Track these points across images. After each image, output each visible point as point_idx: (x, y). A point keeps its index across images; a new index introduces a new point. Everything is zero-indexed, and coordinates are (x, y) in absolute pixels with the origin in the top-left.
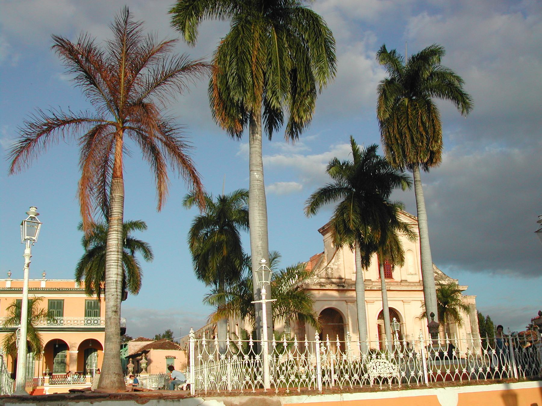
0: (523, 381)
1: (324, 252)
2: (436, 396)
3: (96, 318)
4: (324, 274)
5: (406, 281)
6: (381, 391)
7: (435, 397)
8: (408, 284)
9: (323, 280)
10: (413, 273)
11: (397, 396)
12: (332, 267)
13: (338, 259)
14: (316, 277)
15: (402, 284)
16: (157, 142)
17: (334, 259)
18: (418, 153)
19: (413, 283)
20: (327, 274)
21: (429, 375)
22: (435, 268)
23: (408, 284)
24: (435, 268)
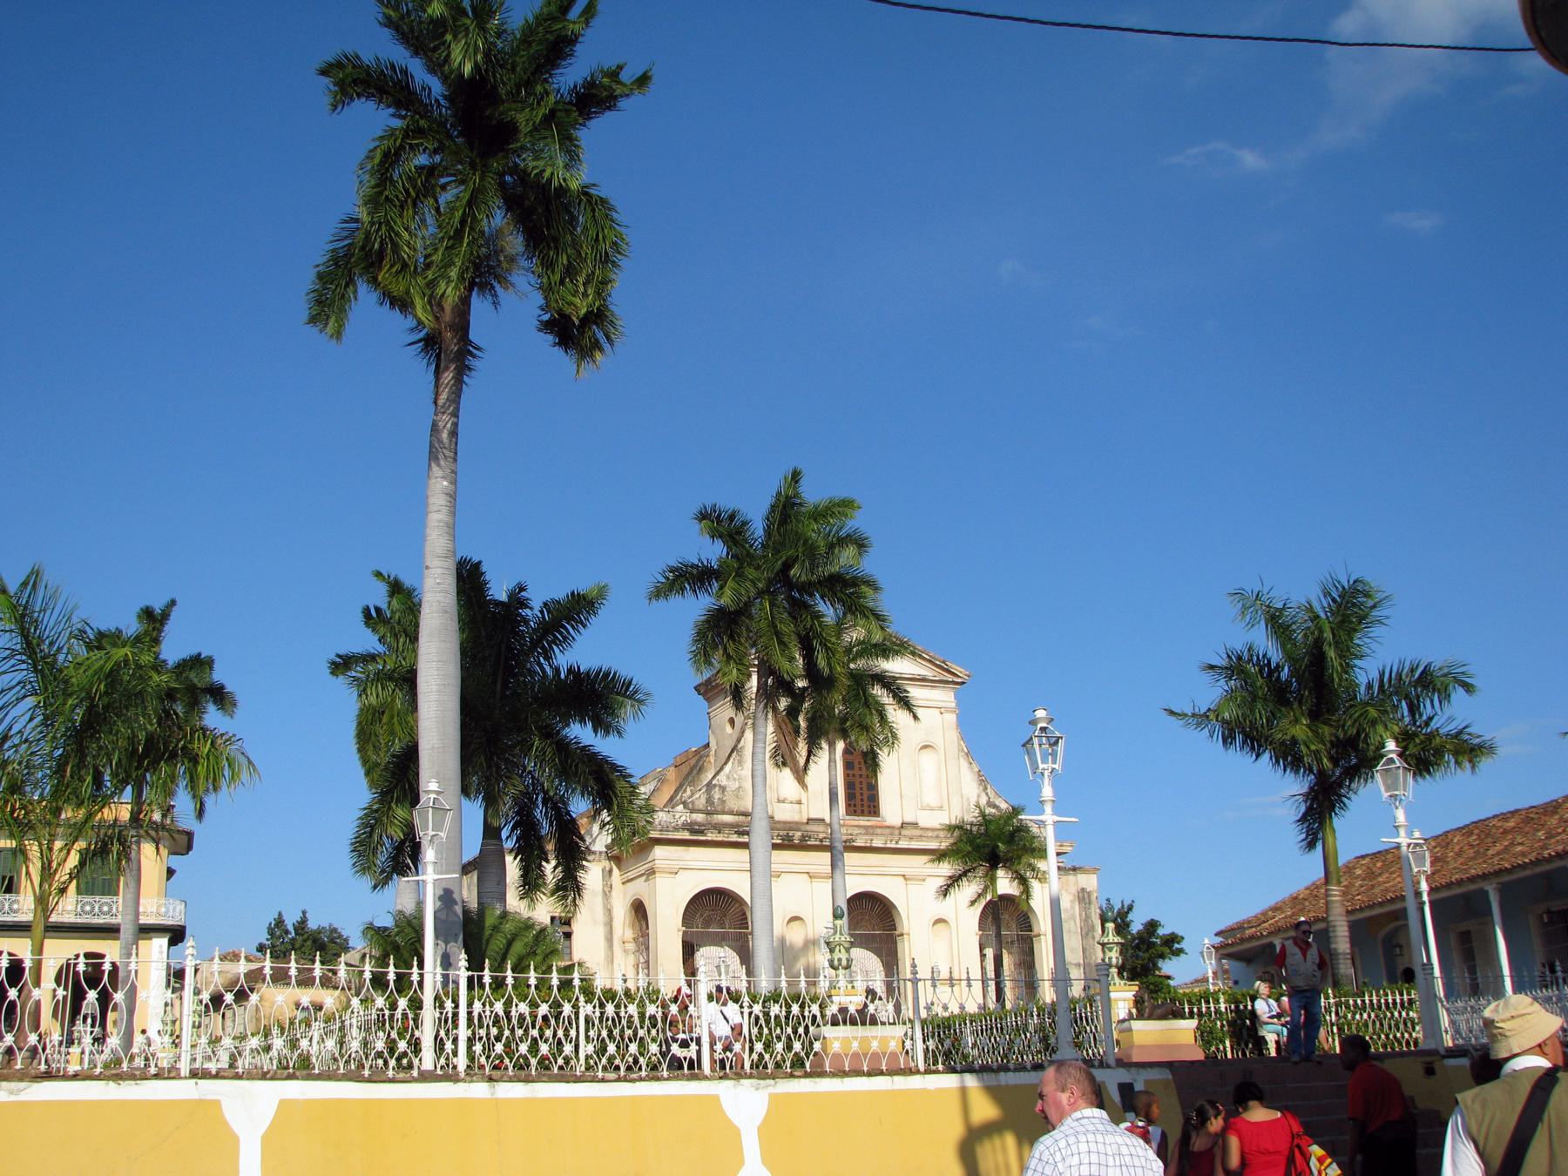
0: (937, 1072)
1: (708, 745)
2: (282, 1102)
3: (106, 899)
4: (703, 800)
5: (915, 825)
6: (511, 1080)
7: (716, 1098)
8: (918, 832)
9: (700, 817)
10: (934, 803)
11: (452, 1095)
12: (724, 783)
13: (740, 763)
14: (680, 807)
15: (904, 832)
16: (450, 300)
17: (730, 764)
18: (784, 506)
19: (933, 830)
20: (709, 800)
21: (926, 1050)
22: (992, 794)
23: (918, 832)
24: (992, 794)
